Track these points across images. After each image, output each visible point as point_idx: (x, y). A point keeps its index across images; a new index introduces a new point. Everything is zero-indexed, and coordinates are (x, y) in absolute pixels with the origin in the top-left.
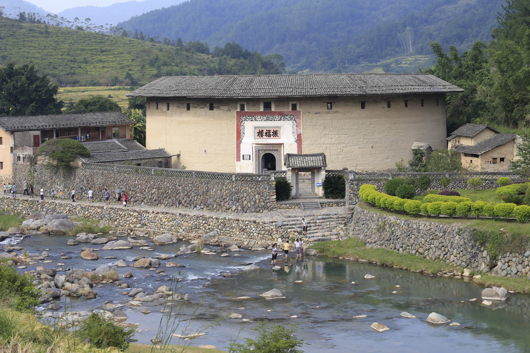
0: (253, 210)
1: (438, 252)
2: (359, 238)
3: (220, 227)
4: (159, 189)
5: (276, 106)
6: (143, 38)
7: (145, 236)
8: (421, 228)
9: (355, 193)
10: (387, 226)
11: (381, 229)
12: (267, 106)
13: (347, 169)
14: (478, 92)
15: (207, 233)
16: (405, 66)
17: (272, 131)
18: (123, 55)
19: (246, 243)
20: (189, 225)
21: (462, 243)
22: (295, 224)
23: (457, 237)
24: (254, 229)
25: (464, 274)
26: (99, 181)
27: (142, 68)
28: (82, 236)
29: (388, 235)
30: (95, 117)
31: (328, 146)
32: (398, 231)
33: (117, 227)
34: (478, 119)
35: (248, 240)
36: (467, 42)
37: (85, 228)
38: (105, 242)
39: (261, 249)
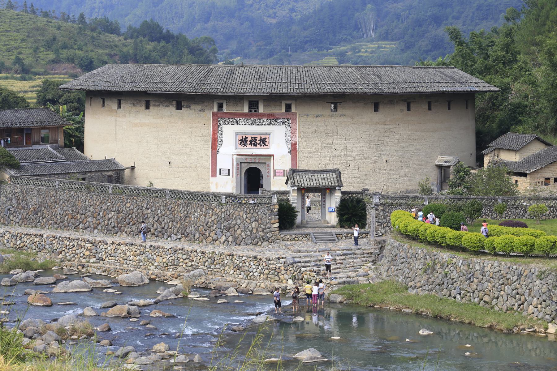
0: (249, 242)
1: (512, 301)
2: (397, 281)
3: (206, 264)
4: (119, 212)
5: (265, 106)
6: (33, 12)
7: (103, 274)
8: (486, 269)
9: (380, 221)
10: (439, 266)
11: (429, 269)
12: (253, 105)
13: (367, 190)
14: (513, 92)
15: (188, 271)
16: (365, 55)
17: (259, 138)
18: (9, 33)
19: (244, 285)
20: (164, 260)
21: (544, 289)
22: (310, 262)
23: (538, 282)
24: (254, 267)
25: (548, 331)
26: (34, 200)
27: (35, 51)
28: (20, 274)
29: (440, 277)
30: (18, 115)
31: (331, 159)
32: (455, 273)
33: (62, 262)
34: (520, 127)
35: (247, 281)
36: (446, 24)
37: (20, 263)
38: (52, 282)
39: (266, 294)
